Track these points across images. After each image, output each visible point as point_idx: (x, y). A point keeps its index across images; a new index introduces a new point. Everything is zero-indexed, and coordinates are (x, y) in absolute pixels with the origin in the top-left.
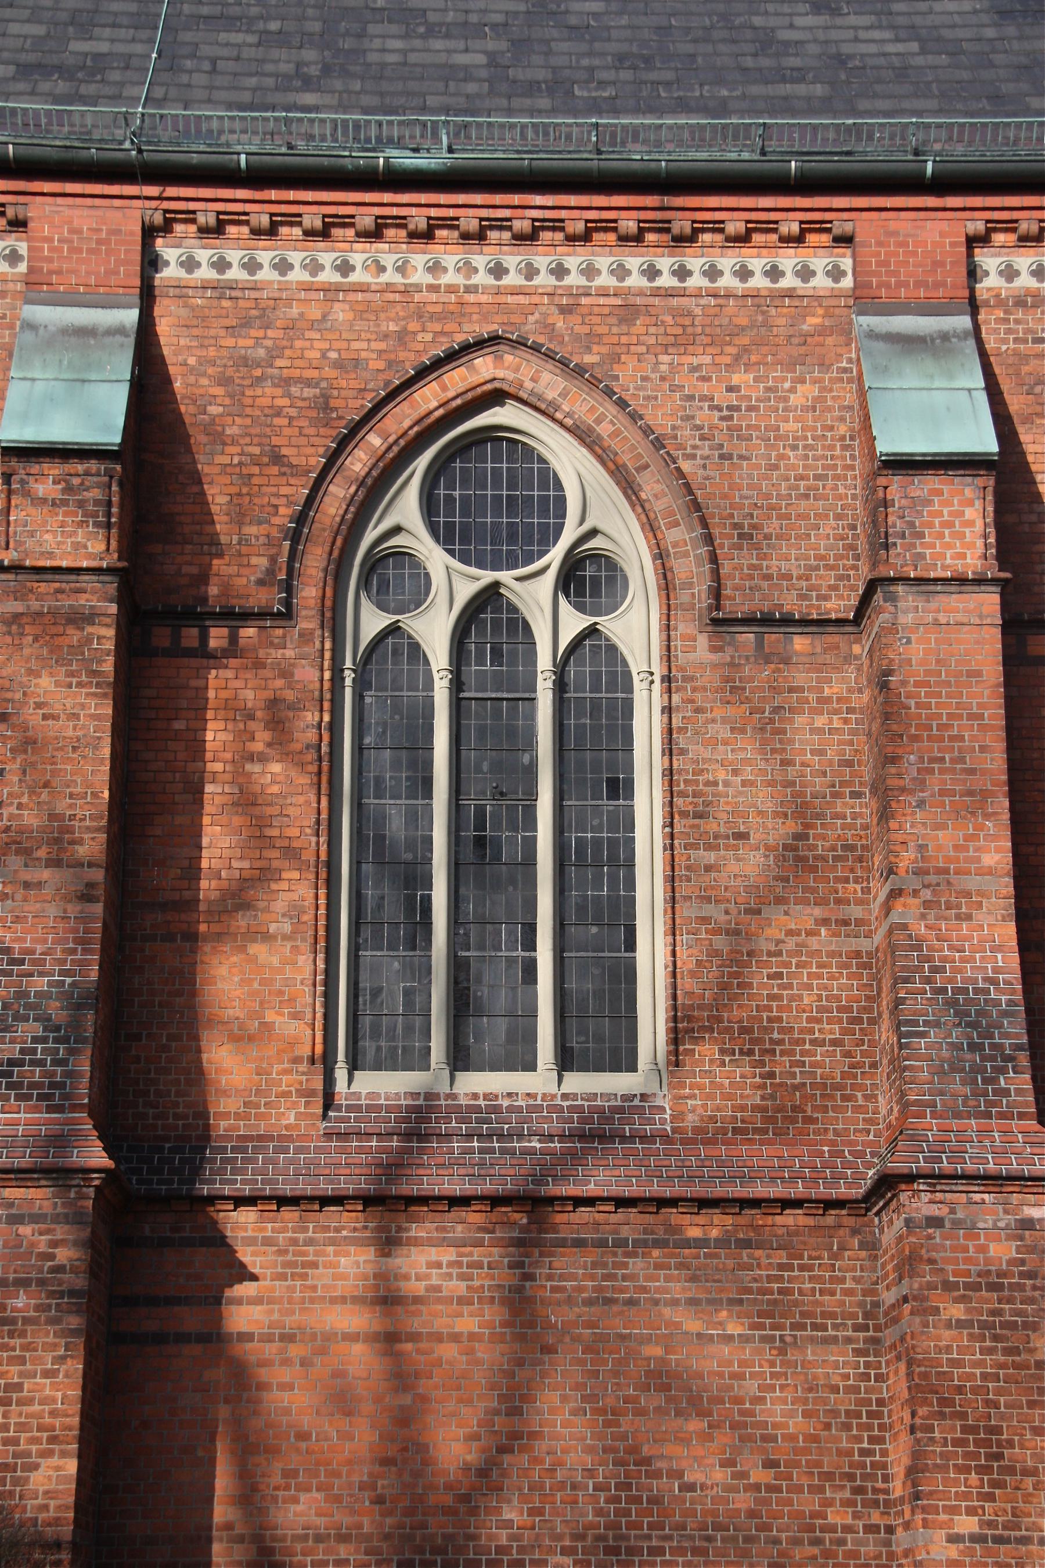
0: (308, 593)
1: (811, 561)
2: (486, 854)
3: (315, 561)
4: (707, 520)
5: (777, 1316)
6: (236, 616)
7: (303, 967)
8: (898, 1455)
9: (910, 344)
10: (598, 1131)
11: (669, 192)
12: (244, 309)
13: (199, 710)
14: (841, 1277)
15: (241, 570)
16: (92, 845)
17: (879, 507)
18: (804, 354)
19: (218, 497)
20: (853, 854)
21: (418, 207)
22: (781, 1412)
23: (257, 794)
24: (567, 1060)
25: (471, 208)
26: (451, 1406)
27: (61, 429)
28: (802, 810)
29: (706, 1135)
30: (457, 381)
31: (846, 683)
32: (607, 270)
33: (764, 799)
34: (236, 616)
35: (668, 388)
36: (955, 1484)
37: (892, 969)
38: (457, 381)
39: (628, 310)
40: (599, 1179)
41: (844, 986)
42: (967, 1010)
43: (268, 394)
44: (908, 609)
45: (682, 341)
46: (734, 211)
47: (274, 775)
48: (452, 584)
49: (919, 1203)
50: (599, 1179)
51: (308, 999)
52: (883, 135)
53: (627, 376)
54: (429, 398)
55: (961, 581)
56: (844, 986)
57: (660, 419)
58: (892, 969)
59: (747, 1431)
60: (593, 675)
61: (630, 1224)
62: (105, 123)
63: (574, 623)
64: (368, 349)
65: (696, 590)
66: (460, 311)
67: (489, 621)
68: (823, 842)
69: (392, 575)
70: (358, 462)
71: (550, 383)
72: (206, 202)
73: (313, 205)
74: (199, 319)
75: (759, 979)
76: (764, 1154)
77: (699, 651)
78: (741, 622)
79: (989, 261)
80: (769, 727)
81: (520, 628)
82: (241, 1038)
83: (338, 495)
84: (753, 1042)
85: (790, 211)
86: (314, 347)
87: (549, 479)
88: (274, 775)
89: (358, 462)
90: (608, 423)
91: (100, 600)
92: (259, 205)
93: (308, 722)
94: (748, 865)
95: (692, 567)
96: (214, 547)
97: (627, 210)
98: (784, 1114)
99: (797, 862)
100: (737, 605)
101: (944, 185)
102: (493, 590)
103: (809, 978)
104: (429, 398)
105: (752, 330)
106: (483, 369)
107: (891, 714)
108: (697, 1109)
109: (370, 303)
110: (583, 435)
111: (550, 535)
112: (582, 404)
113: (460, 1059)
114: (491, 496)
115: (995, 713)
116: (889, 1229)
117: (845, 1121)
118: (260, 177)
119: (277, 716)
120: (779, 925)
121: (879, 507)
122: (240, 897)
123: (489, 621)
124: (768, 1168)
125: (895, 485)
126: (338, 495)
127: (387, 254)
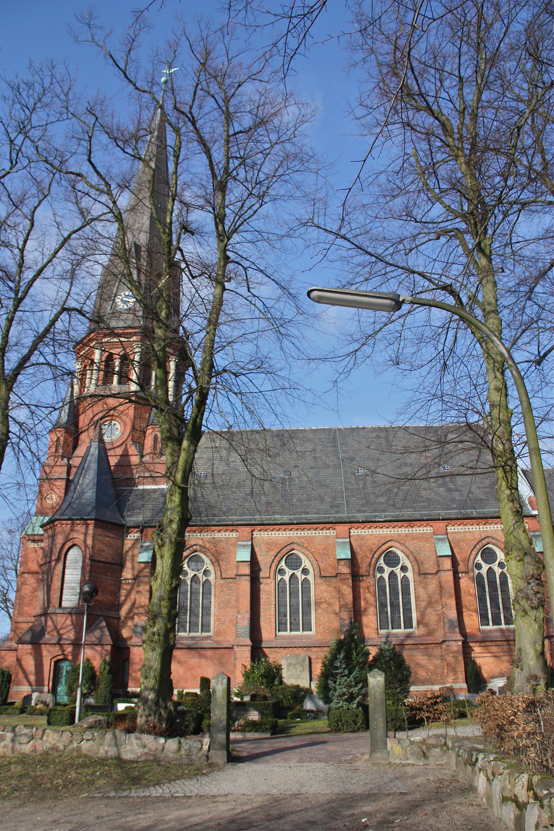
0: (371, 572)
1: (430, 567)
2: (395, 606)
3: (372, 568)
4: (416, 561)
5: (429, 656)
6: (363, 576)
7: (374, 618)
8: (446, 671)
9: (439, 539)
10: (408, 636)
11: (410, 521)
12: (361, 538)
13: (360, 587)
14: (437, 652)
15: (363, 571)
16: (351, 606)
17: (438, 561)
18: (427, 540)
19: (359, 561)
20: (437, 602)
21: (381, 525)
22: (431, 667)
23: (368, 598)
24: (405, 628)
25: (387, 524)
26: (47, 350)
27: (343, 557)
28: (429, 597)
29: (422, 636)
30: (387, 545)
31: (435, 581)
32: (404, 531)
33: (426, 596)
34: (363, 576)
35: (412, 545)
36: (451, 674)
37: (442, 617)
38: (387, 545)
39: (407, 536)
40: (410, 642)
41: (436, 618)
42: (451, 621)
43: (365, 548)
44: (442, 574)
45: (413, 539)
46: (418, 523)
47: (368, 595)
48: (387, 570)
49: (447, 643)
50: (410, 642)
51: (375, 622)
52: (434, 513)
53: (407, 544)
54: (384, 548)
55: (331, 232)
56: (436, 618)
57: (411, 549)
58: (442, 617)
59: (428, 670)
60: (405, 580)
61: (414, 647)
62: (344, 515)
63: (402, 574)
64: (376, 542)
65: (417, 570)
66: (386, 537)
67: (392, 575)
68: (433, 600)
69: (381, 570)
70: (376, 556)
71: (398, 545)
72: (356, 525)
73: (368, 525)
74: (356, 539)
75: (427, 617)
76: (429, 638)
77: (417, 578)
78: (421, 574)
79: (448, 528)
80: (425, 587)
81: (396, 575)
82: (367, 626)
83: (374, 560)
84: (426, 625)
85: (425, 523)
86: (370, 542)
87: (398, 556)
88: (368, 595)
89: (376, 556)
90: (405, 550)
91: (349, 576)
92: (362, 525)
93: (372, 589)
94: (424, 604)
95: (416, 567)
96: (360, 567)
97: (406, 524)
98: (430, 633)
99: (430, 604)
100: (422, 572)
101: (442, 520)
102: (392, 571)
103: (432, 617)
104: (384, 548)
105: (420, 537)
106: (390, 544)
107: (441, 587)
108: (421, 633)
109: (376, 536)
110: (402, 551)
111: (399, 563)
112: (402, 548)
113: (393, 628)
114: (392, 560)
115: (453, 586)
116: (444, 646)
117: (437, 634)
118: (362, 522)
119: (368, 588)
120: (429, 611)
121: (438, 561)
122: (366, 610)
123: (392, 575)
124: (429, 640)
125: (440, 559)
126: (374, 560)
127: (377, 530)
